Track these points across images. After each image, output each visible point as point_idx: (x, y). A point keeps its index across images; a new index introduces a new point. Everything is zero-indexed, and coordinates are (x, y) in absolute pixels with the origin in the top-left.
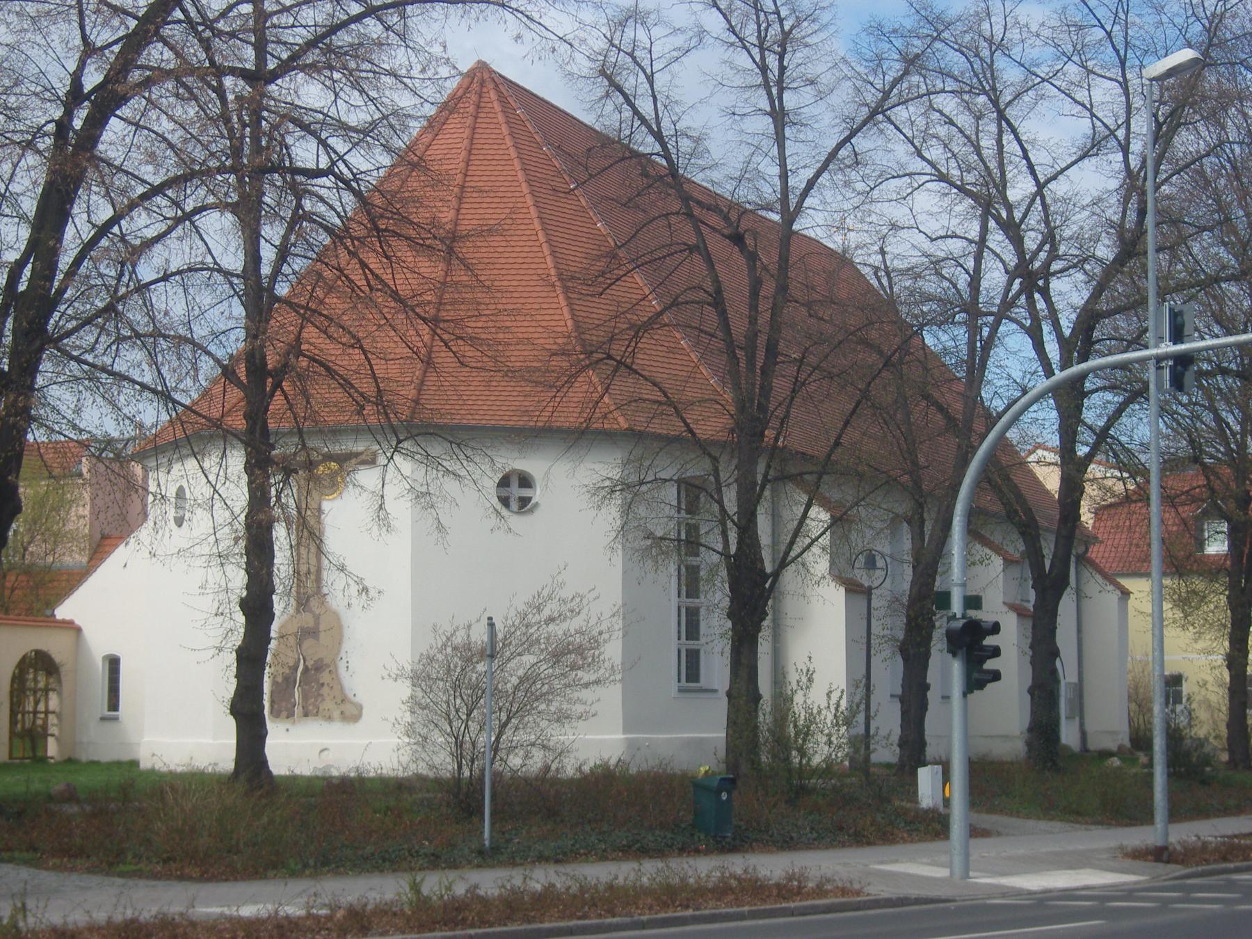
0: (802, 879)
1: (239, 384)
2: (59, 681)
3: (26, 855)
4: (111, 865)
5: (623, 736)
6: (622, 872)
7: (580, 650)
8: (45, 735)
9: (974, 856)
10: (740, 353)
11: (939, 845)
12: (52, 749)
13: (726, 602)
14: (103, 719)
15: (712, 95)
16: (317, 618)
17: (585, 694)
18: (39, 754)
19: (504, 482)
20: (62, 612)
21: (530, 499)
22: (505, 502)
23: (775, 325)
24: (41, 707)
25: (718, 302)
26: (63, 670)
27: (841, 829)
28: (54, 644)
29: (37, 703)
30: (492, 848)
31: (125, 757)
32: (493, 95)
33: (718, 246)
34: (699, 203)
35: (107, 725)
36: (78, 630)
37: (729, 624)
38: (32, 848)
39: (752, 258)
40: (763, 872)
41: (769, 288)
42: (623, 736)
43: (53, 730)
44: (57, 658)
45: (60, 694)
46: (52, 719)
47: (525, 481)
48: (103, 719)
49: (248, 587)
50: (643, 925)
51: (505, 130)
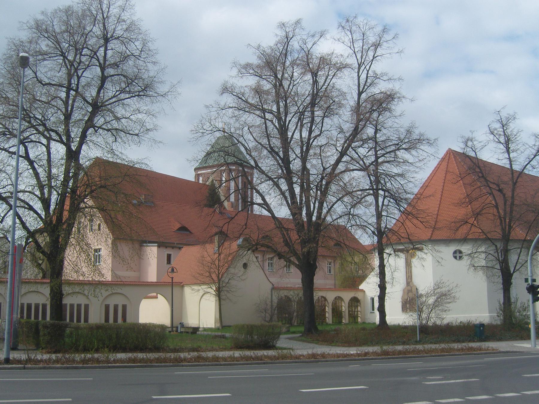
0: (488, 347)
1: (376, 235)
2: (360, 304)
3: (316, 342)
4: (331, 343)
5: (488, 315)
6: (433, 346)
7: (445, 295)
8: (357, 317)
9: (537, 343)
10: (502, 219)
11: (528, 341)
12: (359, 320)
13: (502, 281)
14: (371, 313)
15: (494, 155)
16: (411, 287)
17: (448, 305)
18: (356, 321)
19: (455, 252)
20: (361, 287)
21: (462, 256)
22: (455, 257)
23: (511, 212)
24: (356, 310)
25: (497, 207)
26: (361, 301)
27: (518, 336)
28: (359, 296)
29: (355, 309)
30: (419, 340)
31: (374, 322)
32: (452, 156)
33: (496, 193)
34: (491, 182)
35: (373, 314)
36: (364, 292)
37: (502, 286)
38: (318, 340)
39: (504, 195)
40: (473, 346)
41: (508, 203)
42: (488, 315)
43: (359, 315)
44: (359, 298)
45: (360, 307)
46: (359, 313)
47: (460, 252)
48: (371, 313)
49: (380, 282)
50: (433, 356)
51: (455, 165)
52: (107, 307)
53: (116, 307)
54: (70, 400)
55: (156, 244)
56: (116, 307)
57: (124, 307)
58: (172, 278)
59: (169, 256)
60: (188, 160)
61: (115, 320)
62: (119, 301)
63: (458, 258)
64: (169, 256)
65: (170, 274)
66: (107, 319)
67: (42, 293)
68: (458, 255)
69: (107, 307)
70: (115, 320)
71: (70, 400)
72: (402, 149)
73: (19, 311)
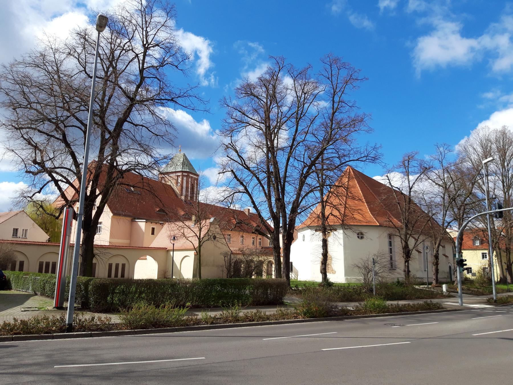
22: (358, 237)
52: (110, 266)
53: (117, 266)
54: (204, 358)
55: (145, 220)
56: (117, 266)
57: (124, 265)
58: (174, 244)
59: (153, 229)
60: (416, 153)
61: (116, 275)
62: (121, 261)
63: (360, 238)
64: (153, 229)
65: (172, 241)
66: (110, 275)
67: (129, 264)
68: (360, 236)
69: (110, 266)
70: (116, 275)
71: (204, 358)
72: (414, 183)
73: (412, 315)
